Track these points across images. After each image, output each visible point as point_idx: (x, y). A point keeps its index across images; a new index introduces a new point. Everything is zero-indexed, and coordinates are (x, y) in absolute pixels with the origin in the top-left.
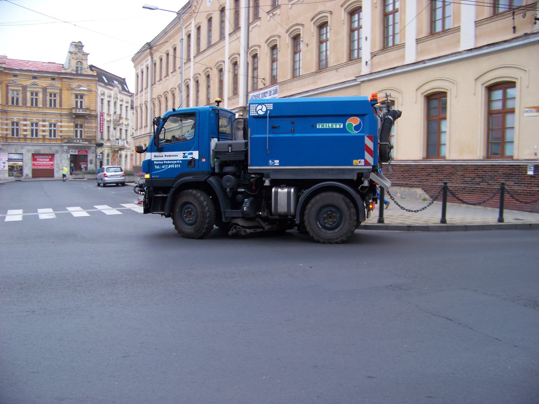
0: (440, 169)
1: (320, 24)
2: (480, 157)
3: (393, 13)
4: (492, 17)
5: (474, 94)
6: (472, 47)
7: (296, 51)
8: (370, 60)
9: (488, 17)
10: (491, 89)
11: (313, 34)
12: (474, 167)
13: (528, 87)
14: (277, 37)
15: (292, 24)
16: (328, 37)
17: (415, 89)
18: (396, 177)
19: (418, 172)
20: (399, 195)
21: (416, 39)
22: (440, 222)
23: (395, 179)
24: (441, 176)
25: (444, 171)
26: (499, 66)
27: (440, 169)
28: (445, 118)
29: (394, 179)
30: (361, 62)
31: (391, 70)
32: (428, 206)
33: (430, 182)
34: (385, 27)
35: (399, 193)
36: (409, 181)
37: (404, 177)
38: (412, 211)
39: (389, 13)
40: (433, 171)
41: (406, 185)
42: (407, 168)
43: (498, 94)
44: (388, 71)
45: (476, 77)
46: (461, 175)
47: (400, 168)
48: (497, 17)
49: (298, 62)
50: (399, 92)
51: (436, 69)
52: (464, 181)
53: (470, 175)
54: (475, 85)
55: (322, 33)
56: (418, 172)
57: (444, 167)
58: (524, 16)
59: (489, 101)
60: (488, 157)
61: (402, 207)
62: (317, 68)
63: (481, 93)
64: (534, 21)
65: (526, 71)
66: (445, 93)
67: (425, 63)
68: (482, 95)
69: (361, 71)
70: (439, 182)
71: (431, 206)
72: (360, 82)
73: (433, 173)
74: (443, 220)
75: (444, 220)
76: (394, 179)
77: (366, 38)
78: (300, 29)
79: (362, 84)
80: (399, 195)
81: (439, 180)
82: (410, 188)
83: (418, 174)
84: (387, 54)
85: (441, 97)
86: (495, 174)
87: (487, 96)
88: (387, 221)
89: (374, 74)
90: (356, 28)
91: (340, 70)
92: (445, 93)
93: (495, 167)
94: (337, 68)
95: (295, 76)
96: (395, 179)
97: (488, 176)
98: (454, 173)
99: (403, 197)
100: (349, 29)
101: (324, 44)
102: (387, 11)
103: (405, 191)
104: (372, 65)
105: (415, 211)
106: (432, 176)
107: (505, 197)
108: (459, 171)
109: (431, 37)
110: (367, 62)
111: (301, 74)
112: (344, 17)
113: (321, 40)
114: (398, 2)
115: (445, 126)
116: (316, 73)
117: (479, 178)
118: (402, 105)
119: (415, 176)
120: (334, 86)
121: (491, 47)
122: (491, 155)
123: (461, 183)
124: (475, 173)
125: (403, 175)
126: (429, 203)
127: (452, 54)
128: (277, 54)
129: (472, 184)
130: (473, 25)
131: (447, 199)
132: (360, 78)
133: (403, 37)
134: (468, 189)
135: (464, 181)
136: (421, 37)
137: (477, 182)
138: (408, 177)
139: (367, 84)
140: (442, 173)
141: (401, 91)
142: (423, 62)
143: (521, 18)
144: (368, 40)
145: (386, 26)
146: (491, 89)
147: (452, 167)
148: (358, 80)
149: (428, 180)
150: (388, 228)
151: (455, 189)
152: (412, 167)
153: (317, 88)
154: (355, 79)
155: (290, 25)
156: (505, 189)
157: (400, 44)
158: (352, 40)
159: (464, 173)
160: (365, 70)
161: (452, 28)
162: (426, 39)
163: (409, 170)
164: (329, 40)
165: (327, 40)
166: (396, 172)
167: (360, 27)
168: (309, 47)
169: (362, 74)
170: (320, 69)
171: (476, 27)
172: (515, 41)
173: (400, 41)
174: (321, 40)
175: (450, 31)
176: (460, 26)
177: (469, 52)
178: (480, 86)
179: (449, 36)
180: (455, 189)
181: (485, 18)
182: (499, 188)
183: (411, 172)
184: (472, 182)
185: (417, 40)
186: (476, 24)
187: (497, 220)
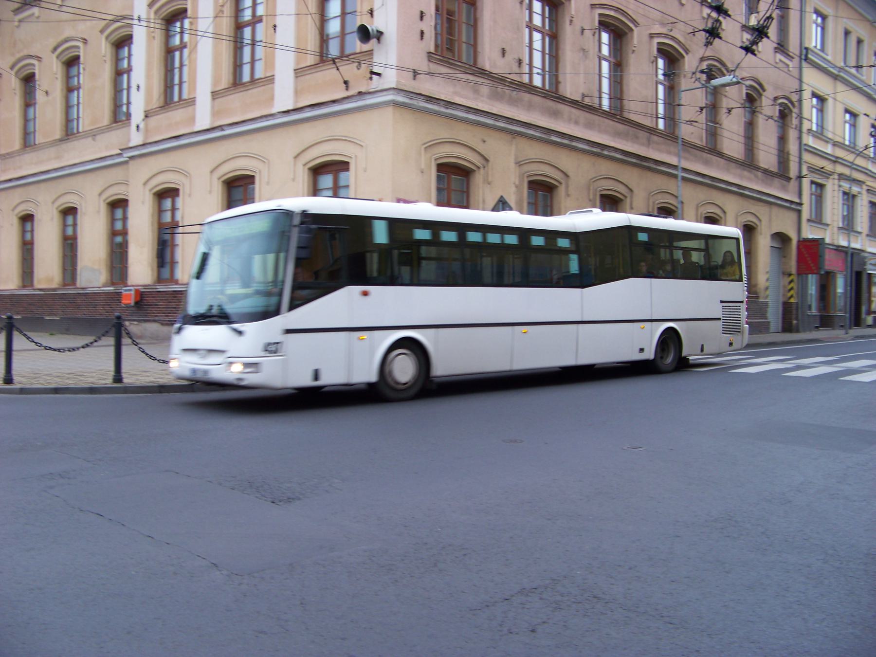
3: (252, 25)
4: (318, 64)
5: (294, 180)
6: (291, 108)
7: (29, 102)
8: (144, 120)
11: (105, 58)
13: (365, 171)
14: (80, 41)
15: (22, 54)
16: (81, 81)
21: (212, 93)
26: (327, 137)
31: (174, 140)
39: (245, 24)
44: (169, 141)
45: (296, 154)
49: (75, 108)
50: (263, 161)
51: (240, 141)
54: (295, 165)
55: (121, 56)
58: (359, 67)
62: (64, 133)
64: (369, 75)
65: (362, 146)
66: (253, 177)
67: (223, 130)
68: (303, 181)
69: (129, 141)
77: (138, 87)
78: (33, 65)
84: (170, 113)
85: (339, 170)
87: (225, 195)
88: (127, 380)
90: (247, 23)
91: (98, 137)
92: (253, 177)
94: (93, 134)
95: (27, 145)
100: (114, 70)
101: (76, 93)
102: (241, 20)
104: (147, 131)
110: (138, 127)
111: (81, 130)
112: (106, 52)
116: (61, 140)
121: (316, 109)
128: (78, 76)
130: (291, 74)
132: (127, 151)
133: (193, 87)
142: (221, 128)
143: (355, 69)
145: (169, 69)
148: (125, 155)
155: (18, 56)
158: (118, 89)
160: (136, 139)
164: (188, 46)
165: (78, 89)
167: (129, 70)
168: (50, 98)
169: (131, 145)
170: (67, 135)
171: (297, 77)
172: (347, 101)
173: (189, 94)
174: (70, 85)
176: (273, 76)
178: (301, 167)
181: (309, 64)
185: (296, 71)
186: (296, 73)
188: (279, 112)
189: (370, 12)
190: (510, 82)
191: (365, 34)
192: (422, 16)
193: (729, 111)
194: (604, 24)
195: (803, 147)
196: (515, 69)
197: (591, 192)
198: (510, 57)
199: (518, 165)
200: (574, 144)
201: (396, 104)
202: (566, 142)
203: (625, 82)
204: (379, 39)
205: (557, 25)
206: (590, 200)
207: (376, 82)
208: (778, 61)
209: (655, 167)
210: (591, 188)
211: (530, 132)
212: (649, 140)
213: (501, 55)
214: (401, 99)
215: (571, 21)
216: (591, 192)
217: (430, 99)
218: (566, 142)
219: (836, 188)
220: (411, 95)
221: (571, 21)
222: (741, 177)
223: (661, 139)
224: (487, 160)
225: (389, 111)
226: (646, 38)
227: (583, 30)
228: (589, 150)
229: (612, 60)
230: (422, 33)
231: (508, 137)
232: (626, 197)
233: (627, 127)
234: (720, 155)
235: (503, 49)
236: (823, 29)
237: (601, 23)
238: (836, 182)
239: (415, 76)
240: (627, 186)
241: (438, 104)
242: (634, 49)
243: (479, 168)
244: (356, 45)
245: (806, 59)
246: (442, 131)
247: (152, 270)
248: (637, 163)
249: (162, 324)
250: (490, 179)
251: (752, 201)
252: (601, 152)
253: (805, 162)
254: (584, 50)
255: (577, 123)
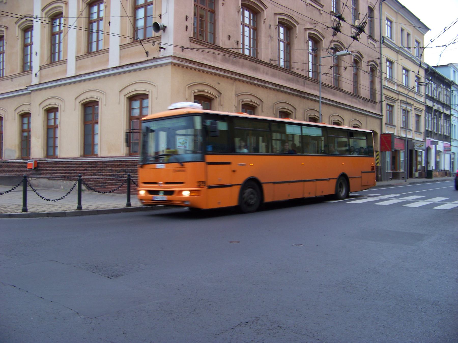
0: (94, 165)
1: (25, 27)
2: (123, 154)
3: (59, 34)
4: (132, 43)
6: (74, 75)
9: (129, 43)
10: (131, 99)
12: (119, 163)
16: (5, 49)
17: (74, 98)
18: (60, 172)
19: (77, 168)
20: (62, 187)
22: (76, 209)
23: (59, 174)
24: (95, 171)
25: (97, 166)
27: (94, 165)
28: (97, 123)
29: (58, 174)
30: (32, 74)
32: (66, 196)
33: (86, 176)
34: (53, 45)
35: (63, 186)
36: (70, 175)
37: (66, 172)
38: (52, 201)
40: (88, 166)
41: (68, 179)
42: (68, 165)
43: (136, 104)
44: (53, 82)
45: (120, 90)
46: (110, 169)
47: (62, 165)
48: (135, 43)
50: (5, 111)
51: (91, 82)
52: (112, 174)
53: (116, 169)
54: (120, 96)
55: (27, 37)
56: (77, 168)
57: (97, 163)
58: (154, 45)
59: (130, 109)
60: (130, 154)
61: (43, 197)
63: (124, 102)
64: (159, 49)
65: (155, 86)
66: (98, 102)
67: (82, 77)
69: (31, 82)
70: (93, 176)
71: (68, 195)
72: (30, 91)
73: (88, 168)
74: (80, 207)
75: (80, 207)
76: (58, 174)
79: (32, 93)
80: (62, 187)
81: (94, 174)
82: (70, 181)
83: (77, 169)
86: (134, 168)
87: (83, 111)
89: (42, 85)
91: (14, 80)
92: (98, 102)
93: (134, 162)
94: (12, 78)
96: (59, 174)
97: (130, 169)
98: (105, 168)
99: (65, 189)
100: (50, 33)
102: (91, 19)
103: (67, 184)
104: (41, 76)
105: (55, 201)
106: (88, 171)
107: (131, 186)
108: (108, 166)
109: (87, 55)
110: (36, 74)
113: (26, 43)
114: (103, 11)
115: (98, 128)
117: (123, 171)
118: (64, 111)
119: (75, 171)
120: (9, 93)
121: (139, 65)
122: (132, 152)
123: (110, 176)
124: (120, 168)
125: (65, 171)
126: (66, 193)
127: (102, 70)
129: (118, 176)
131: (127, 190)
134: (115, 181)
135: (112, 174)
136: (80, 55)
137: (122, 174)
138: (69, 172)
139: (36, 93)
140: (95, 168)
141: (63, 99)
142: (80, 76)
144: (37, 54)
146: (131, 99)
147: (103, 163)
148: (29, 89)
149: (85, 174)
150: (30, 215)
151: (105, 180)
152: (72, 163)
153: (17, 90)
154: (26, 89)
156: (131, 179)
157: (63, 60)
158: (25, 54)
159: (112, 168)
160: (35, 81)
161: (103, 49)
162: (127, 46)
163: (70, 166)
164: (5, 53)
166: (59, 168)
167: (31, 44)
169: (32, 84)
173: (64, 58)
175: (101, 52)
176: (161, 36)
177: (115, 69)
178: (123, 97)
179: (101, 55)
180: (105, 180)
181: (127, 43)
182: (126, 178)
183: (71, 168)
184: (118, 174)
185: (76, 58)
187: (126, 205)
188: (111, 68)
189: (159, 16)
190: (232, 53)
191: (157, 27)
192: (187, 18)
193: (345, 68)
194: (282, 23)
195: (383, 87)
196: (235, 46)
197: (275, 110)
198: (233, 40)
199: (237, 96)
200: (266, 85)
201: (173, 64)
202: (261, 84)
203: (292, 53)
204: (164, 30)
205: (257, 24)
206: (274, 114)
207: (163, 53)
208: (369, 43)
209: (307, 96)
210: (275, 108)
211: (243, 79)
212: (304, 83)
213: (228, 39)
214: (175, 61)
215: (264, 22)
216: (275, 110)
217: (191, 62)
218: (261, 84)
219: (399, 107)
220: (181, 59)
221: (264, 22)
222: (352, 102)
223: (310, 82)
224: (220, 93)
225: (170, 67)
226: (302, 31)
227: (270, 26)
228: (273, 88)
229: (285, 42)
230: (187, 27)
231: (231, 81)
232: (292, 112)
233: (293, 76)
234: (341, 90)
235: (229, 35)
236: (391, 27)
237: (279, 22)
238: (399, 104)
239: (183, 50)
240: (293, 106)
241: (195, 64)
242: (297, 36)
243: (216, 97)
244: (152, 33)
245: (383, 42)
246: (197, 78)
247: (44, 150)
248: (298, 95)
249: (49, 179)
250: (222, 103)
251: (357, 114)
252: (280, 89)
253: (384, 94)
254: (271, 36)
255: (267, 74)
